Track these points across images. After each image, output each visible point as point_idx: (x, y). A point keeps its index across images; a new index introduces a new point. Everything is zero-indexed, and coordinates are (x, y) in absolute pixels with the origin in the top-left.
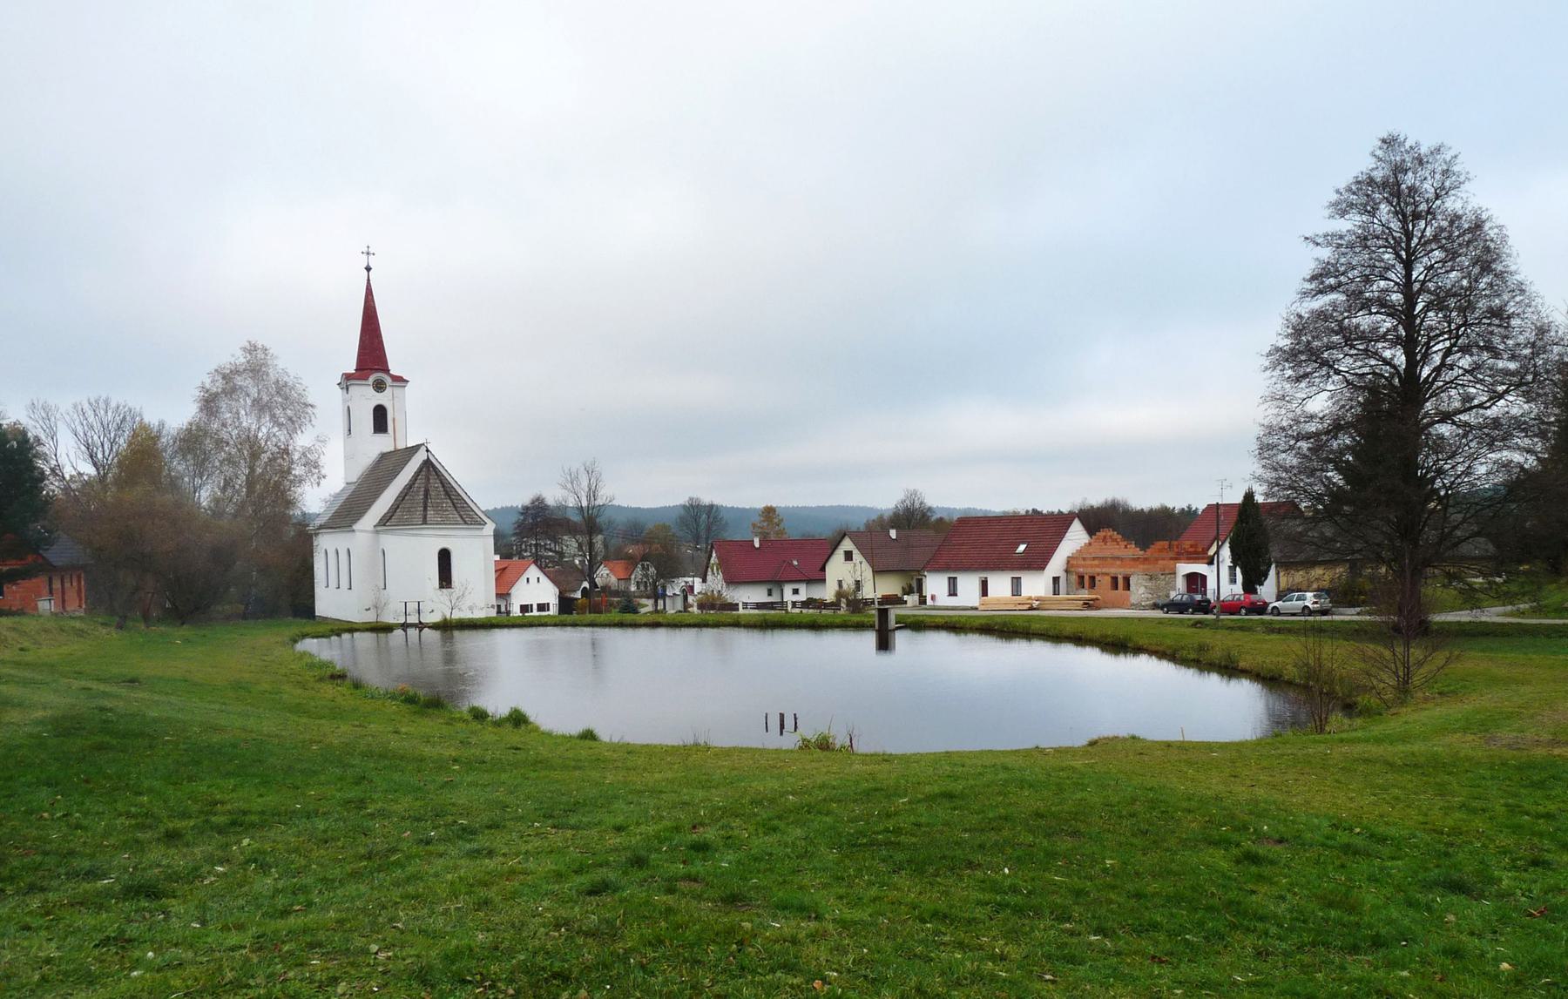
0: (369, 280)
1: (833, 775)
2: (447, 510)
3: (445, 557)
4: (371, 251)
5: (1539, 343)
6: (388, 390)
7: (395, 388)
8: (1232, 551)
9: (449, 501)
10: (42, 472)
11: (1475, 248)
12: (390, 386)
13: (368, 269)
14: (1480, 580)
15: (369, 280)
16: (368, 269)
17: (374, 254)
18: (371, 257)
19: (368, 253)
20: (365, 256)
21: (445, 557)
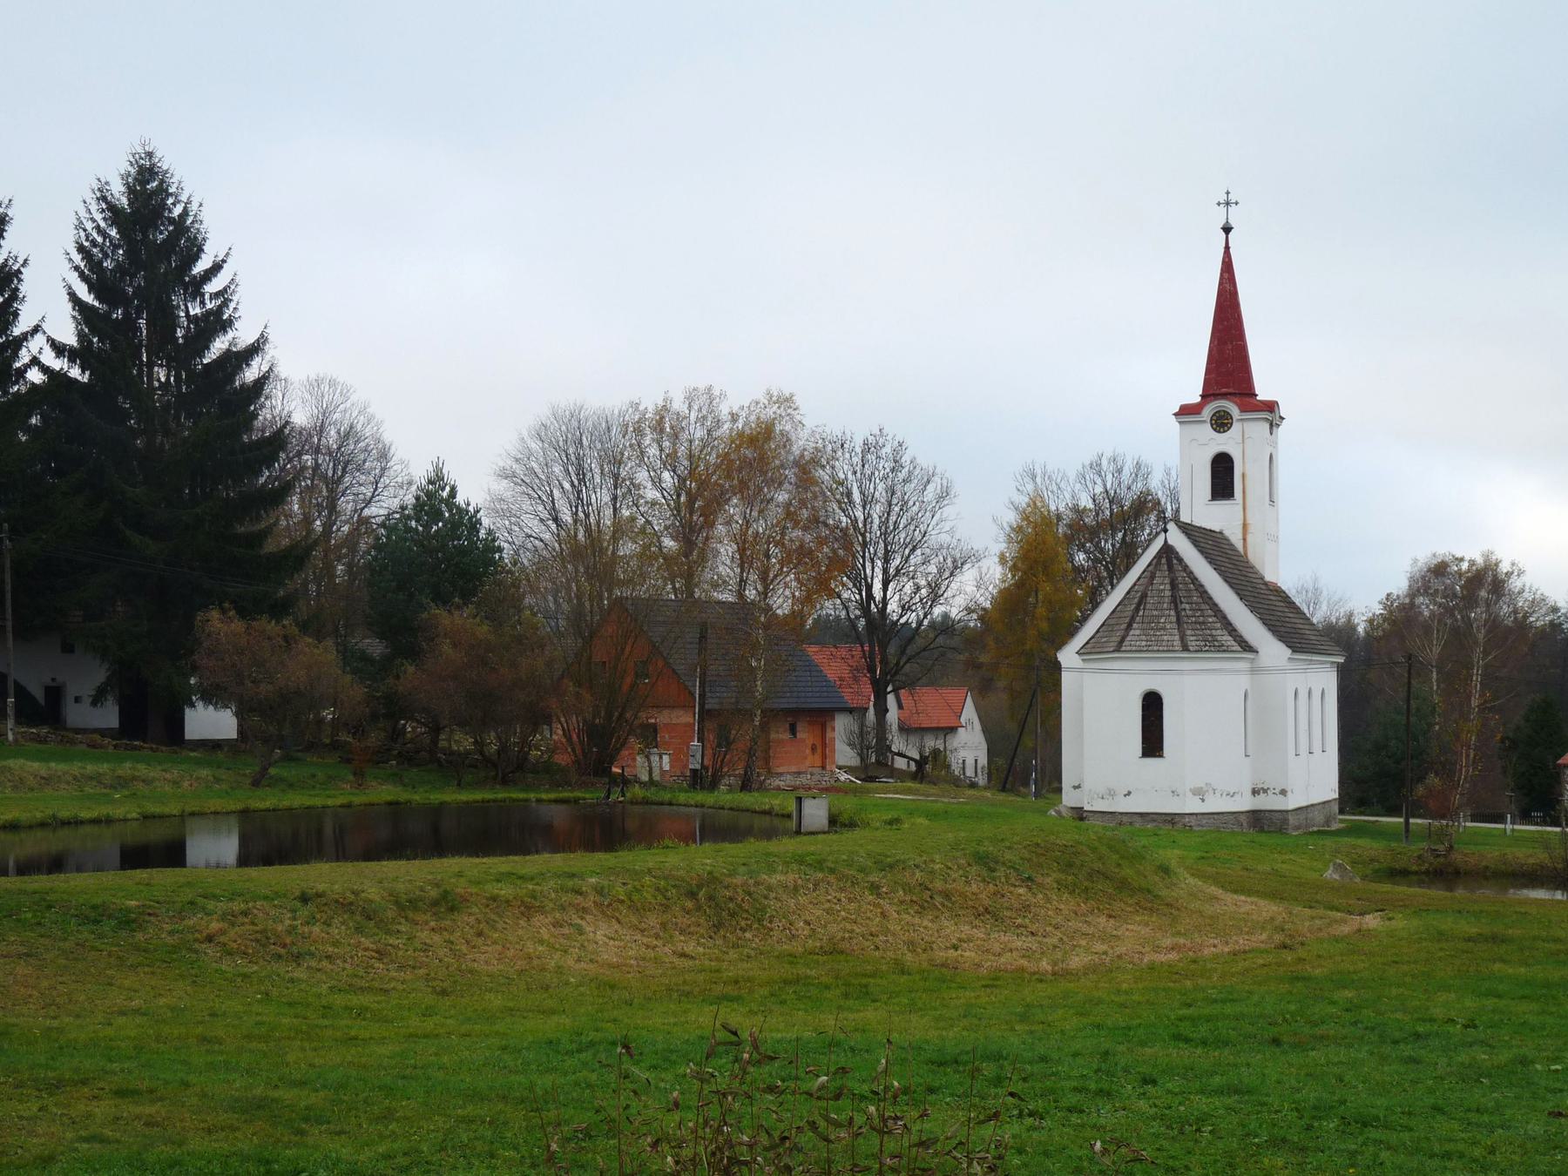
0: (1227, 248)
1: (607, 498)
2: (1164, 629)
3: (1152, 705)
4: (1233, 198)
5: (1055, 885)
6: (1236, 427)
7: (1245, 424)
8: (33, 698)
9: (1173, 613)
10: (1551, 622)
11: (978, 997)
12: (1238, 420)
13: (1227, 229)
14: (672, 543)
15: (1227, 248)
16: (1227, 229)
17: (1228, 193)
18: (1233, 208)
19: (1228, 204)
20: (1223, 209)
21: (1152, 705)
